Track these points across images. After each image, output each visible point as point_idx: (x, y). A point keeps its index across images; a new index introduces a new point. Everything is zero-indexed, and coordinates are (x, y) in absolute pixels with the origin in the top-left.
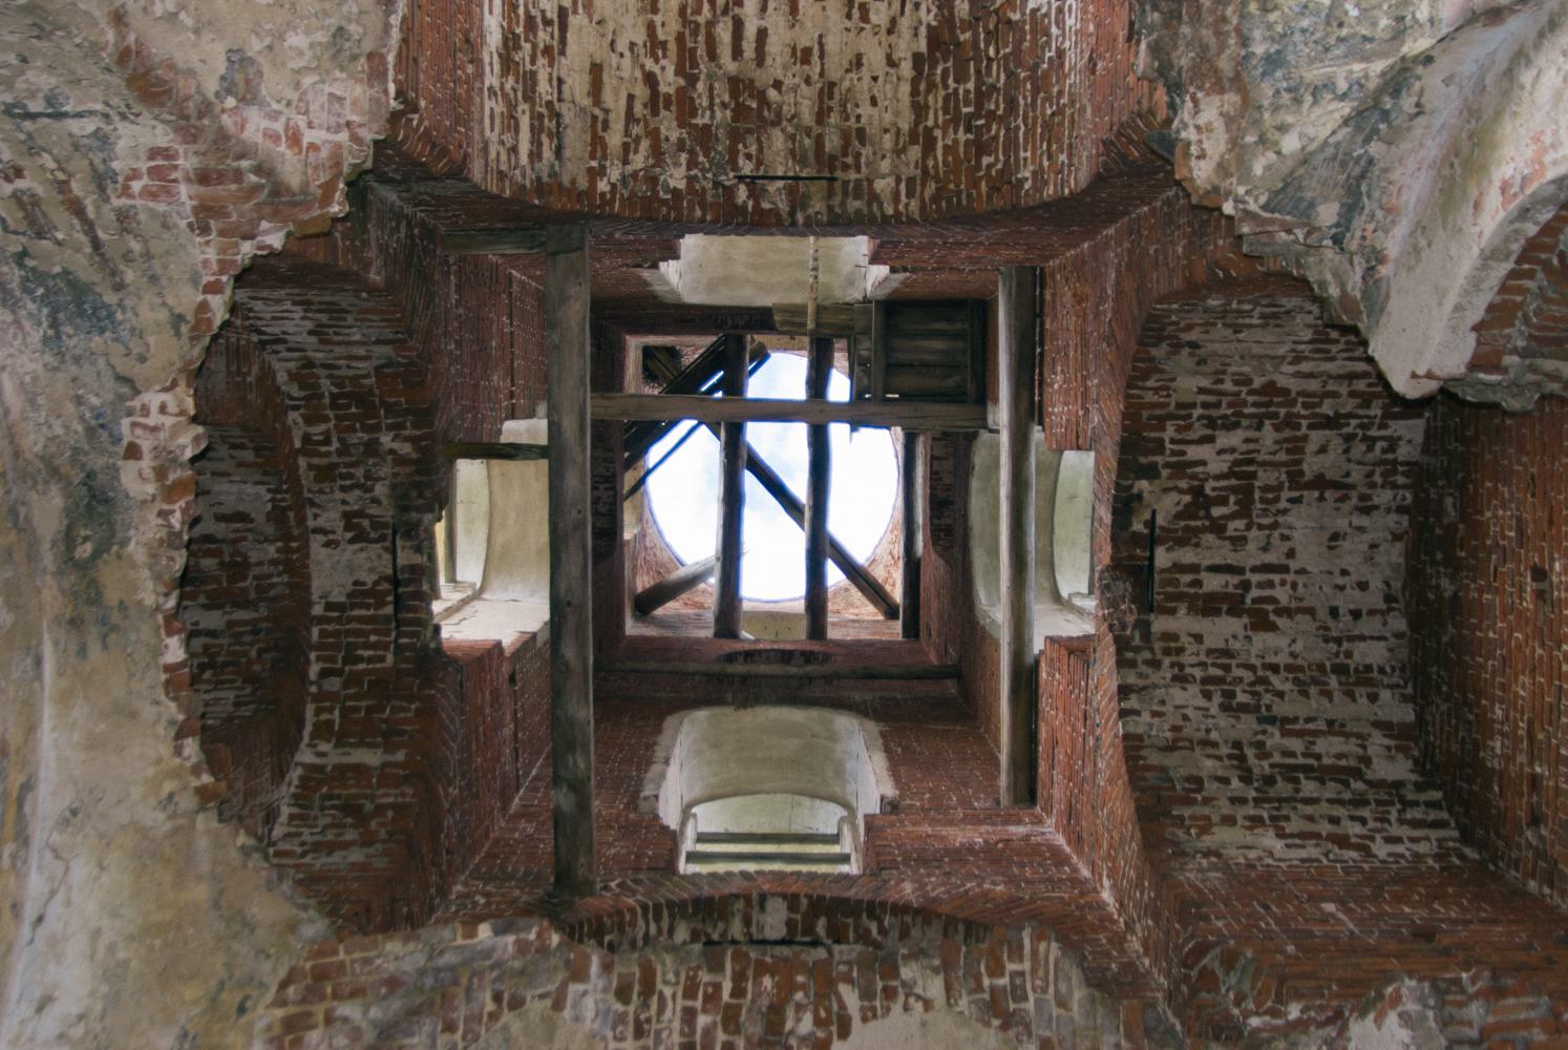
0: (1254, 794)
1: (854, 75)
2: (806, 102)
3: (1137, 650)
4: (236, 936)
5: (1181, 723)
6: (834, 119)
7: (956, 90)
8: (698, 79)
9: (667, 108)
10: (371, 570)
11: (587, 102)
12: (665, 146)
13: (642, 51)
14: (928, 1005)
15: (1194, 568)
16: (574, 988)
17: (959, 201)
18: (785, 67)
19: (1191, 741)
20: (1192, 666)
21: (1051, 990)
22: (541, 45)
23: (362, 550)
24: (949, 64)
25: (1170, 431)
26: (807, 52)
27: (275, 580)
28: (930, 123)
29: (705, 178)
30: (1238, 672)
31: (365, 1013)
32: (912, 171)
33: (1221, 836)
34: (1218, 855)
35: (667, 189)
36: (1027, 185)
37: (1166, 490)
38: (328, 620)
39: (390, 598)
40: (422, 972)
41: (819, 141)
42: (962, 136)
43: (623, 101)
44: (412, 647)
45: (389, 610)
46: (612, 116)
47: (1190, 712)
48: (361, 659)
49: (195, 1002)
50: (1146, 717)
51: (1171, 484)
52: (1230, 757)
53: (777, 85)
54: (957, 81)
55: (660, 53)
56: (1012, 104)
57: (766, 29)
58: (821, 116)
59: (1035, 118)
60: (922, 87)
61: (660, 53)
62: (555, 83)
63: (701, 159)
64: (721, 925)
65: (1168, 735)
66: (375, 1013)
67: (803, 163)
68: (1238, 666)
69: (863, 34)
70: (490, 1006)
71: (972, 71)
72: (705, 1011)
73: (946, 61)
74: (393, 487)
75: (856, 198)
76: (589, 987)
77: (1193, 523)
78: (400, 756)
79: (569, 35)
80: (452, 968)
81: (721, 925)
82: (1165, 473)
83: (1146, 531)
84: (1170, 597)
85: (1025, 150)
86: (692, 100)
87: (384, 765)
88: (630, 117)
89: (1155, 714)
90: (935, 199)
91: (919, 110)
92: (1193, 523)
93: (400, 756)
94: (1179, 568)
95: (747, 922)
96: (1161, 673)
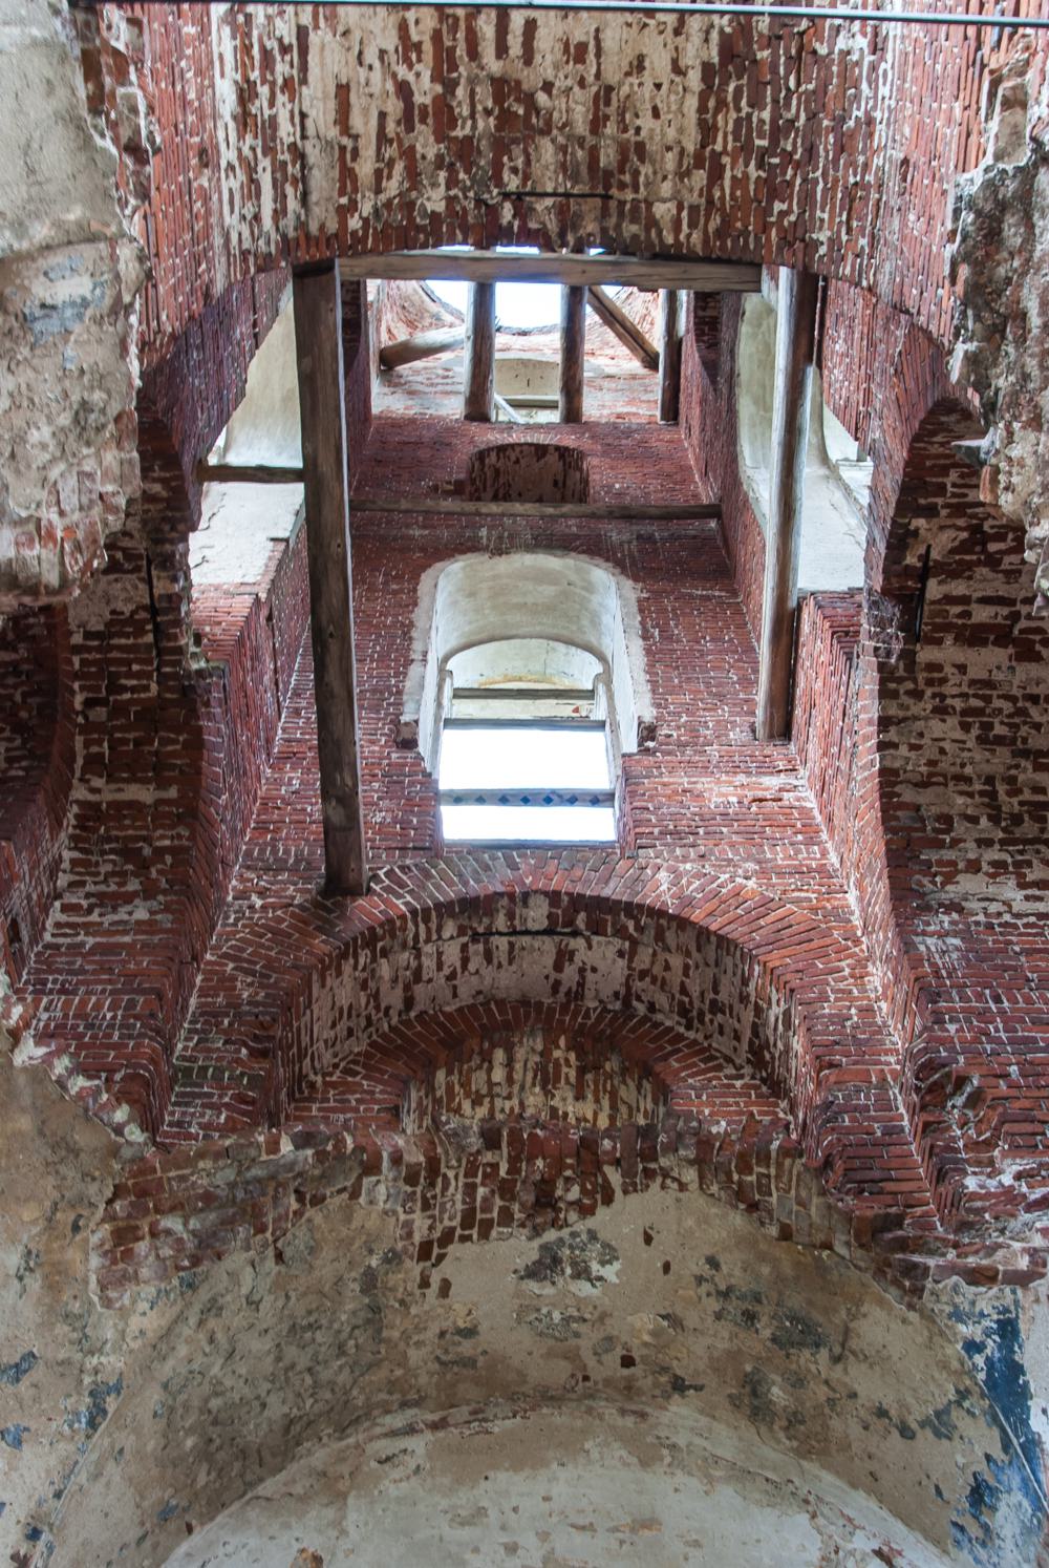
0: (1001, 835)
1: (634, 80)
2: (580, 109)
3: (900, 680)
4: (62, 1161)
5: (938, 757)
6: (610, 129)
7: (749, 116)
8: (458, 84)
9: (423, 121)
10: (128, 600)
11: (333, 132)
12: (421, 166)
13: (393, 58)
14: (683, 1187)
15: (964, 600)
16: (367, 1181)
17: (746, 242)
18: (556, 67)
19: (945, 776)
20: (953, 697)
21: (793, 1192)
22: (280, 81)
23: (116, 580)
24: (744, 81)
25: (953, 476)
26: (582, 48)
27: (32, 620)
28: (718, 147)
29: (466, 197)
30: (997, 703)
31: (185, 1224)
32: (694, 198)
33: (967, 884)
34: (960, 910)
35: (424, 213)
36: (823, 250)
37: (942, 528)
38: (89, 650)
39: (149, 627)
40: (232, 1186)
41: (593, 154)
42: (754, 172)
43: (374, 122)
44: (175, 676)
45: (149, 638)
46: (361, 142)
47: (947, 745)
48: (125, 689)
49: (34, 1222)
50: (903, 750)
51: (949, 522)
52: (982, 793)
53: (548, 87)
54: (751, 105)
55: (414, 57)
56: (811, 152)
57: (534, 21)
58: (596, 125)
59: (836, 180)
60: (712, 103)
61: (414, 57)
62: (297, 120)
63: (462, 176)
64: (486, 920)
65: (923, 769)
66: (194, 1223)
67: (575, 178)
68: (999, 697)
69: (646, 31)
70: (294, 1205)
71: (769, 100)
72: (483, 1184)
73: (739, 78)
74: (144, 522)
75: (634, 220)
76: (382, 1178)
77: (967, 557)
78: (172, 793)
79: (310, 58)
80: (258, 1180)
81: (486, 920)
82: (944, 512)
83: (919, 565)
84: (938, 628)
85: (823, 211)
86: (451, 108)
87: (159, 802)
88: (382, 138)
89: (913, 747)
90: (721, 233)
91: (707, 130)
92: (967, 557)
93: (172, 793)
94: (949, 599)
95: (511, 916)
96: (922, 705)
